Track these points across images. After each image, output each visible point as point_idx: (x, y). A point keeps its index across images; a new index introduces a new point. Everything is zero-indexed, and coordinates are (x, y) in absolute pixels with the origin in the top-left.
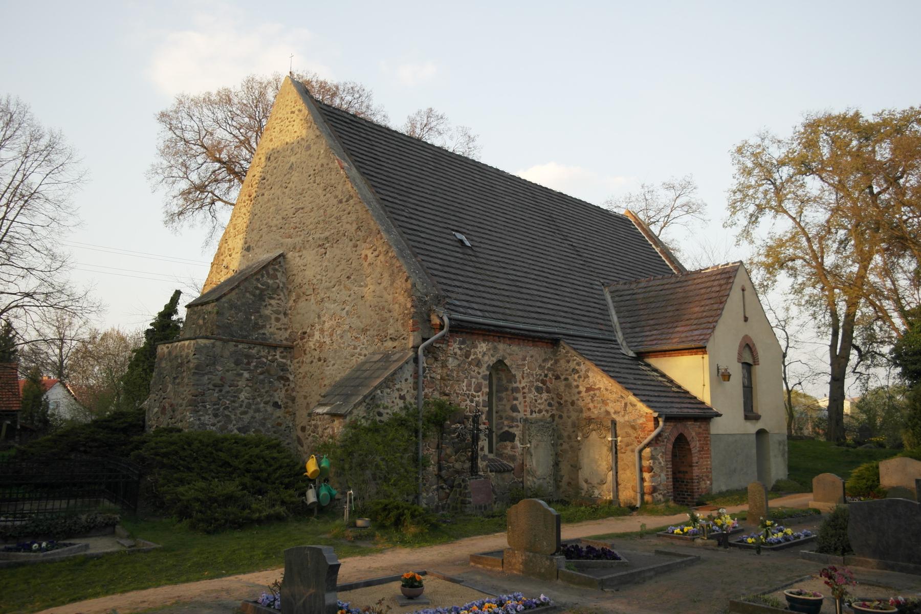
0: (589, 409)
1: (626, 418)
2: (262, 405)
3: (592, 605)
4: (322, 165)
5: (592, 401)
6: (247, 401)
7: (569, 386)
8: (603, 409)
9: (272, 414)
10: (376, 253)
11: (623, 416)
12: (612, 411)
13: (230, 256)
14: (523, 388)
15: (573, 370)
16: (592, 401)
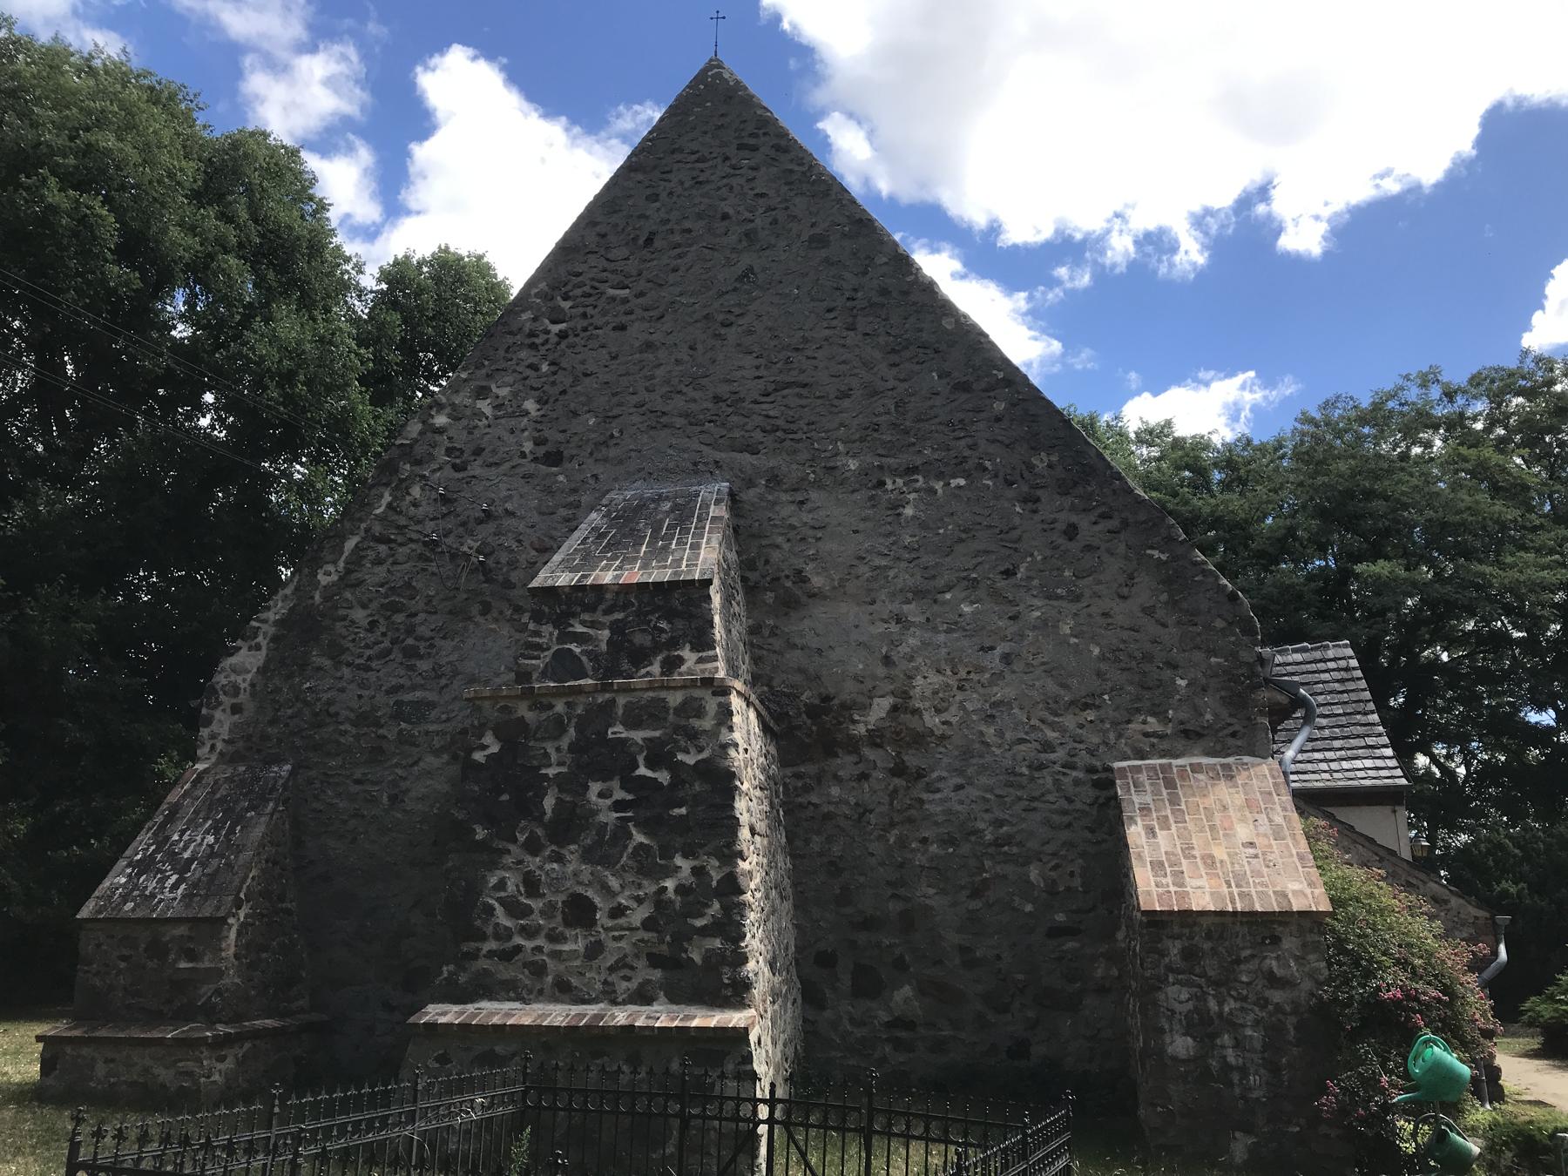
3: (712, 1023)
10: (1114, 523)
13: (456, 468)
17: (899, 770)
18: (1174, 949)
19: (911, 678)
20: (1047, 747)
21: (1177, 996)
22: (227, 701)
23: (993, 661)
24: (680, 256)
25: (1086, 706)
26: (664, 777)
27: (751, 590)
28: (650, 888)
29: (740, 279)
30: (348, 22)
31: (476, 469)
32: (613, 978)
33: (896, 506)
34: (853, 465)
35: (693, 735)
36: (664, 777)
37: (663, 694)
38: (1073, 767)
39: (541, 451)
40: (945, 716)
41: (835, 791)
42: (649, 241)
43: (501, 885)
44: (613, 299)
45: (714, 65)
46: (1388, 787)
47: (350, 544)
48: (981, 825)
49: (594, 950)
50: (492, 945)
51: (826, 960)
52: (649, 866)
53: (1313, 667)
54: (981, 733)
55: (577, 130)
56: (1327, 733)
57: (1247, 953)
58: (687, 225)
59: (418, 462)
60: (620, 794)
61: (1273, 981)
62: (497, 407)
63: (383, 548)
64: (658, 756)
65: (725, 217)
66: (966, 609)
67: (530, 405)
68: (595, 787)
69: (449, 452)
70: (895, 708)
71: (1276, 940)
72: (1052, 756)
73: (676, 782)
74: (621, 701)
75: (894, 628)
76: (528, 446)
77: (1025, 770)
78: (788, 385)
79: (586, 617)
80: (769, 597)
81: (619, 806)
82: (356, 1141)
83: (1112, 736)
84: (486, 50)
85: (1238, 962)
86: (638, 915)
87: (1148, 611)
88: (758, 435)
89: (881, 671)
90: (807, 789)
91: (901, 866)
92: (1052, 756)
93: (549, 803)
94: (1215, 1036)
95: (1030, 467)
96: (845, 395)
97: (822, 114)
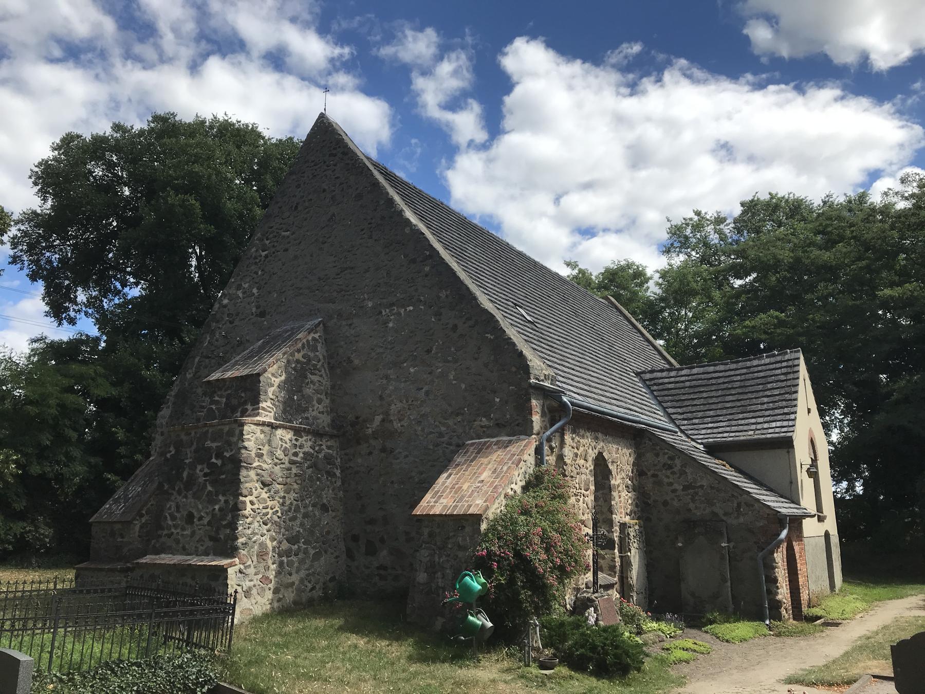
0: (690, 510)
1: (741, 520)
2: (310, 508)
3: (213, 563)
4: (383, 218)
5: (693, 500)
6: (295, 503)
7: (659, 483)
8: (708, 510)
9: (320, 520)
10: (471, 323)
11: (737, 518)
12: (721, 513)
13: (231, 323)
14: (618, 486)
15: (664, 465)
16: (693, 500)
17: (383, 450)
18: (426, 531)
19: (390, 405)
20: (441, 435)
21: (424, 555)
22: (159, 430)
23: (422, 394)
24: (308, 212)
25: (457, 415)
26: (219, 462)
27: (332, 368)
28: (211, 509)
29: (329, 220)
30: (457, 40)
31: (237, 323)
32: (198, 545)
33: (385, 323)
34: (370, 304)
35: (229, 444)
36: (219, 462)
37: (222, 427)
38: (450, 444)
39: (259, 310)
40: (402, 423)
41: (360, 461)
42: (296, 207)
43: (170, 508)
44: (284, 236)
45: (322, 116)
46: (755, 440)
47: (197, 360)
48: (413, 474)
49: (193, 533)
50: (165, 532)
51: (355, 538)
52: (212, 501)
53: (774, 366)
54: (415, 430)
55: (587, 65)
56: (765, 406)
57: (451, 534)
58: (310, 197)
59: (218, 322)
60: (206, 470)
61: (460, 548)
62: (244, 293)
63: (207, 360)
64: (219, 455)
65: (324, 191)
66: (412, 370)
67: (255, 291)
68: (199, 467)
69: (228, 315)
70: (383, 420)
71: (463, 527)
72: (442, 440)
73: (223, 464)
74: (210, 431)
75: (385, 381)
76: (254, 310)
77: (431, 447)
78: (346, 269)
79: (219, 393)
80: (338, 371)
81: (205, 475)
82: (165, 610)
83: (467, 428)
84: (532, 35)
85: (448, 538)
86: (206, 521)
87: (486, 365)
88: (335, 294)
89: (378, 403)
90: (350, 460)
91: (384, 494)
92: (442, 440)
93: (185, 475)
94: (435, 573)
95: (439, 297)
96: (367, 271)
97: (743, 22)
